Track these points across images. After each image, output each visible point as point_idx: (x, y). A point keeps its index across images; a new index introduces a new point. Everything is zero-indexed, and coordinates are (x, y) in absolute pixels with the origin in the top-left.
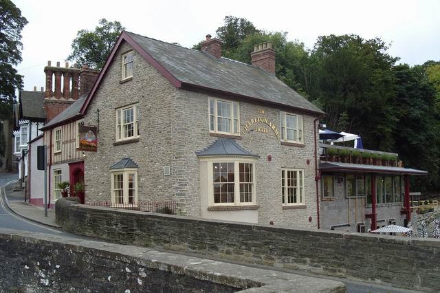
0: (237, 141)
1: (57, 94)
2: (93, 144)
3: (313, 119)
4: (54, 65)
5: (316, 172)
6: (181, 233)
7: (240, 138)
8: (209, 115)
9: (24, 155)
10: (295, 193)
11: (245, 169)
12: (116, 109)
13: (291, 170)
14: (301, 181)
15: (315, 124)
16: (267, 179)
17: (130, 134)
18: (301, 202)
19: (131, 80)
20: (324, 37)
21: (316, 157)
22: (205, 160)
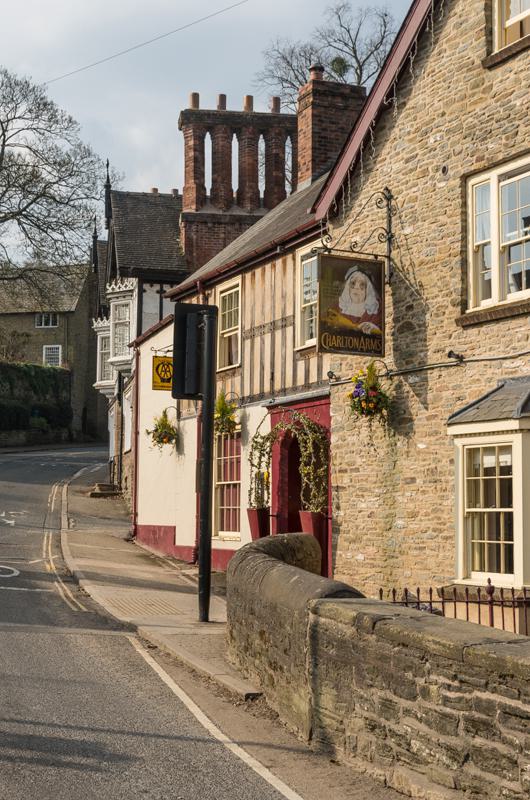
2: (370, 327)
4: (209, 104)
9: (122, 387)
12: (465, 178)
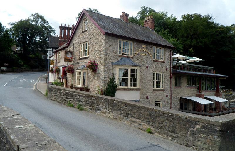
0: (132, 59)
1: (64, 38)
2: (71, 59)
3: (170, 50)
4: (63, 25)
5: (170, 74)
6: (87, 101)
7: (133, 58)
8: (119, 47)
10: (160, 84)
11: (134, 72)
12: (80, 44)
13: (157, 73)
14: (163, 78)
15: (170, 53)
16: (145, 77)
17: (85, 55)
18: (162, 88)
19: (86, 30)
20: (184, 15)
21: (170, 67)
22: (116, 67)
